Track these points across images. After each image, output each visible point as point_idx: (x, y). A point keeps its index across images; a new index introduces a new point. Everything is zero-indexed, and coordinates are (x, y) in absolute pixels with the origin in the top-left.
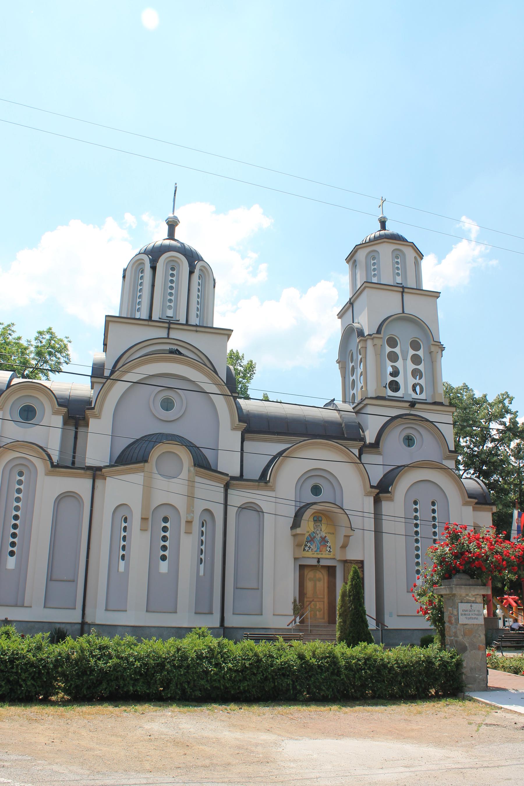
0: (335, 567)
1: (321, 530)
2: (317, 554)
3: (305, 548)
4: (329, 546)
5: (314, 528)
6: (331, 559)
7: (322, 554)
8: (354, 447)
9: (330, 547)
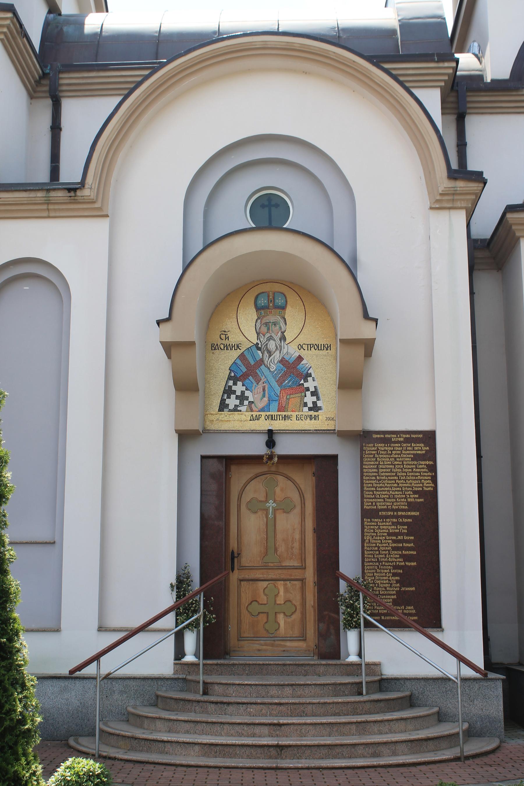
0: (334, 458)
1: (283, 338)
2: (267, 418)
3: (228, 401)
4: (312, 389)
5: (258, 334)
6: (317, 432)
7: (285, 418)
8: (426, 84)
9: (314, 394)
